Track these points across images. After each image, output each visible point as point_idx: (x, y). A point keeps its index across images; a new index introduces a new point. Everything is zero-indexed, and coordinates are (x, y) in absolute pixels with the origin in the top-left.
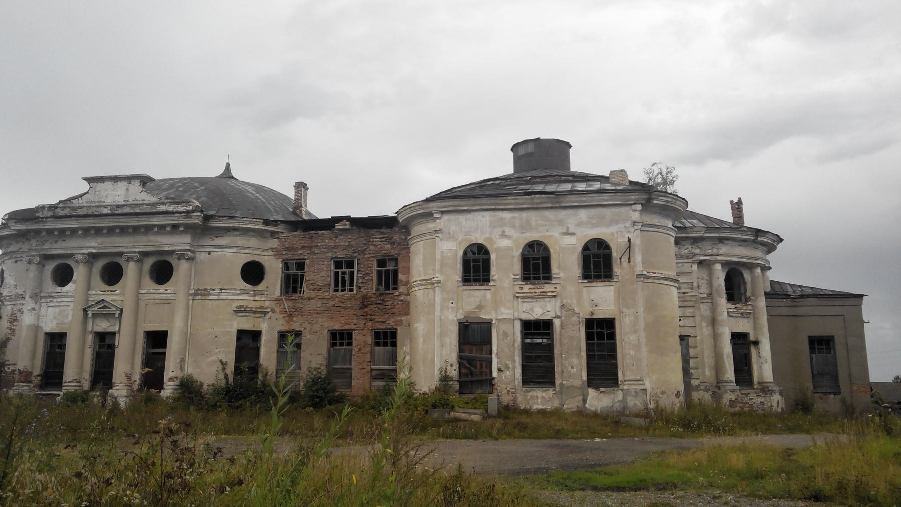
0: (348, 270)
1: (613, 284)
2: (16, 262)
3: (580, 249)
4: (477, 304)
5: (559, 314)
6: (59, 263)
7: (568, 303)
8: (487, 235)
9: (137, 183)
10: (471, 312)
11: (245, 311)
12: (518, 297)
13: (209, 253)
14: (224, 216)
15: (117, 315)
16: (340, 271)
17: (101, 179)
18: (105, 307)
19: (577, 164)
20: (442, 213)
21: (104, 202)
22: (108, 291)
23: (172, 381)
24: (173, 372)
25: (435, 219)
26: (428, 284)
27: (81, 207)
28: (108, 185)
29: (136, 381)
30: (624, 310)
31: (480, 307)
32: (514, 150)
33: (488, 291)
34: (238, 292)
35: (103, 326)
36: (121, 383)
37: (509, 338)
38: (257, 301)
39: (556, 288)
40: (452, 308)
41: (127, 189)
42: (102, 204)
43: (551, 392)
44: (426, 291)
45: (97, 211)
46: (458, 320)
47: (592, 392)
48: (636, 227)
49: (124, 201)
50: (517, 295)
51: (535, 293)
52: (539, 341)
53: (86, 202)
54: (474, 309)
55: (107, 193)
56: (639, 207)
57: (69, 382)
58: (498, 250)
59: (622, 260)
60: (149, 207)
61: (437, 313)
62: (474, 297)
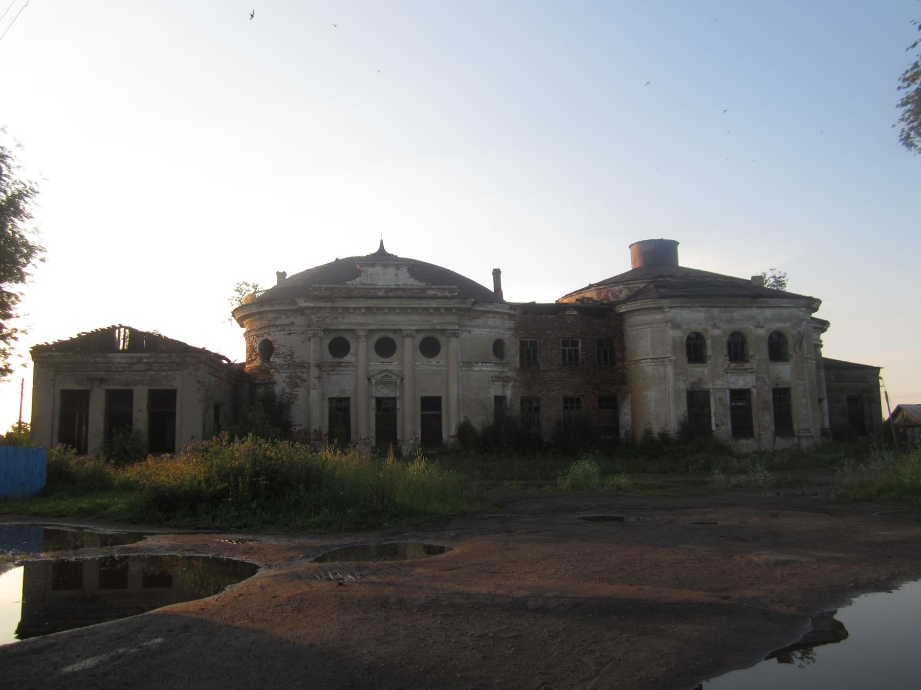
0: (573, 348)
2: (290, 334)
3: (767, 338)
5: (755, 385)
6: (331, 338)
8: (704, 326)
12: (727, 373)
13: (470, 332)
14: (485, 302)
15: (398, 383)
16: (567, 349)
20: (671, 307)
21: (376, 284)
22: (386, 362)
25: (665, 312)
29: (418, 438)
32: (631, 247)
33: (705, 368)
35: (384, 392)
36: (411, 440)
39: (752, 366)
40: (683, 380)
41: (397, 274)
43: (752, 440)
47: (778, 439)
49: (395, 285)
52: (740, 404)
53: (360, 284)
56: (804, 309)
58: (712, 337)
59: (796, 346)
60: (420, 291)
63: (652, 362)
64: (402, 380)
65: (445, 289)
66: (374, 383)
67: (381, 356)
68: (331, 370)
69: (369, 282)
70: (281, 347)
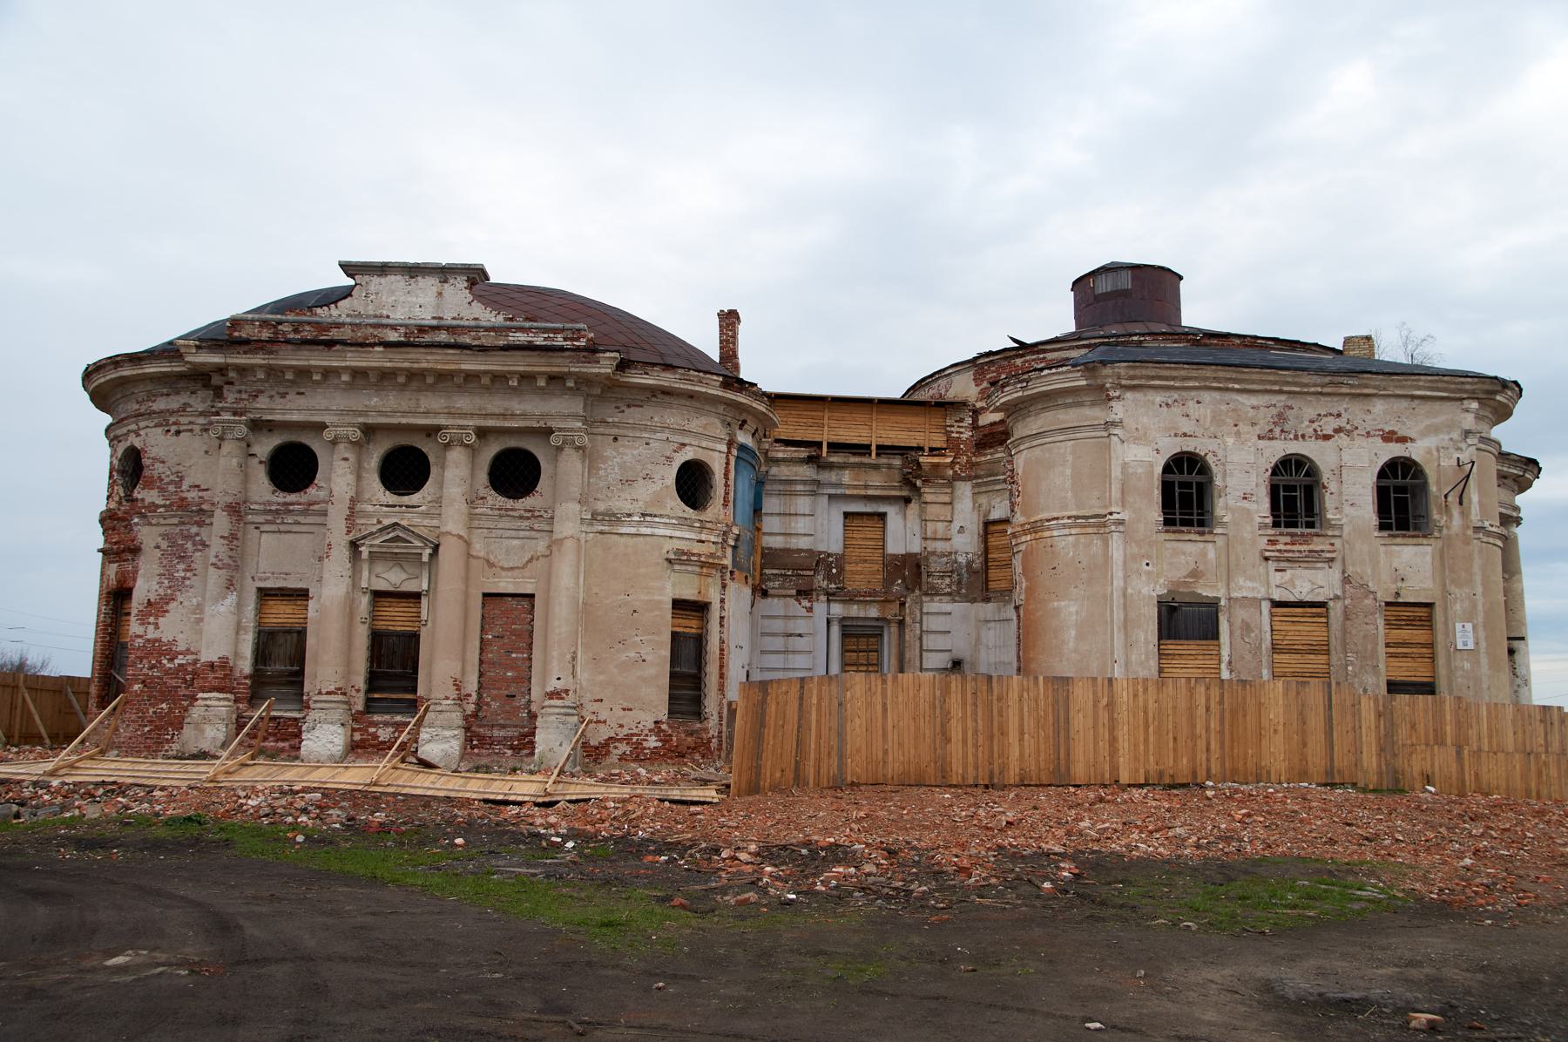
1: (1431, 541)
2: (178, 433)
4: (1191, 569)
5: (1339, 593)
7: (1357, 573)
9: (461, 282)
10: (1179, 583)
11: (688, 562)
12: (1267, 559)
14: (654, 365)
15: (425, 558)
17: (383, 269)
18: (397, 539)
19: (1196, 313)
23: (557, 698)
24: (559, 679)
26: (1089, 526)
27: (338, 325)
28: (396, 281)
29: (470, 695)
30: (1452, 588)
31: (1195, 574)
33: (1210, 545)
34: (674, 521)
36: (447, 698)
37: (1253, 635)
38: (703, 542)
39: (1332, 544)
40: (1149, 573)
41: (440, 294)
42: (385, 321)
44: (1082, 539)
45: (375, 336)
46: (1158, 596)
48: (1469, 441)
49: (434, 318)
50: (1267, 554)
51: (1300, 552)
53: (348, 316)
54: (1185, 577)
55: (393, 298)
57: (329, 693)
59: (1449, 499)
61: (1118, 583)
62: (1184, 553)
63: (1076, 527)
64: (436, 548)
65: (555, 331)
66: (365, 555)
67: (509, 497)
68: (268, 522)
69: (371, 310)
70: (157, 465)
